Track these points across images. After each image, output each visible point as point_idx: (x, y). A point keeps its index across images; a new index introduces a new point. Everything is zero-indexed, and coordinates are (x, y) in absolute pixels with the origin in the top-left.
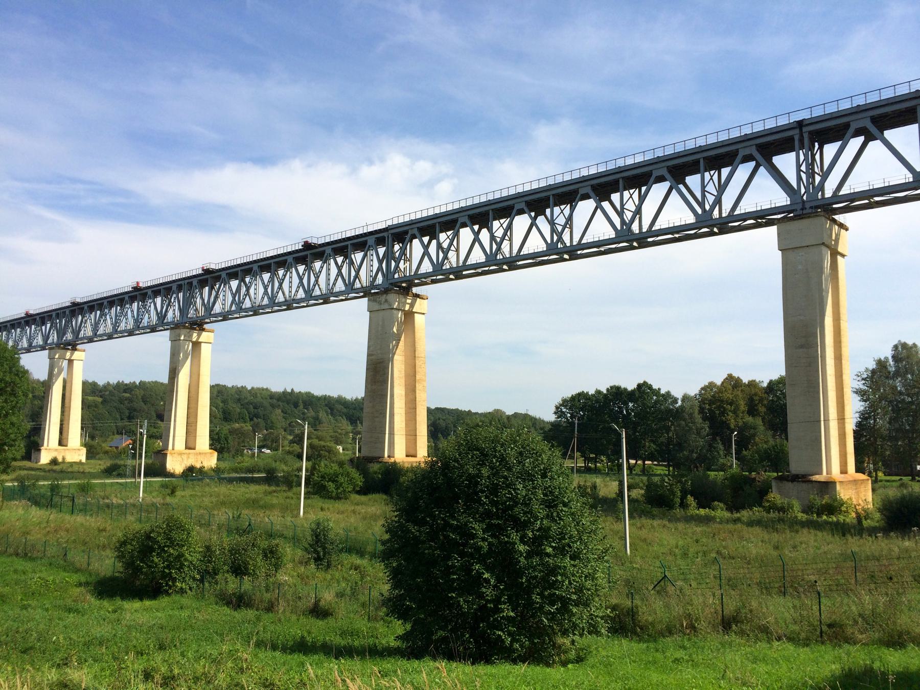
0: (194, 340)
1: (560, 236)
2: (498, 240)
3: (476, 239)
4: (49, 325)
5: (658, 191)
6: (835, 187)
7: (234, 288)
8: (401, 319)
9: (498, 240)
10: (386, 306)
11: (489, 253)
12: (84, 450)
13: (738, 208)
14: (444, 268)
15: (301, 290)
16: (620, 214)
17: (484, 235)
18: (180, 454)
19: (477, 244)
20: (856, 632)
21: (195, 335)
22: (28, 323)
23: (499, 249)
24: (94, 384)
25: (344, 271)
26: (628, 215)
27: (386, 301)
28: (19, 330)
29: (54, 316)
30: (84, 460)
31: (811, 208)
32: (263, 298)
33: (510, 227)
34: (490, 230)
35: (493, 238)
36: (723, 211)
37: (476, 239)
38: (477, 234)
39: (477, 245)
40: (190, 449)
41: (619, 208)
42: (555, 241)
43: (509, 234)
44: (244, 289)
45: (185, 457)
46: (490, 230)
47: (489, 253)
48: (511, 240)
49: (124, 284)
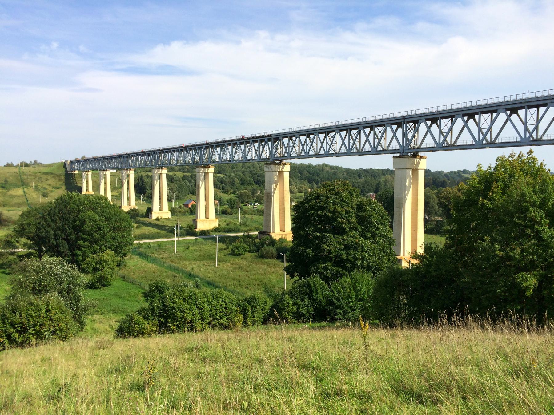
0: (206, 172)
1: (531, 134)
2: (445, 134)
3: (429, 131)
4: (151, 156)
5: (503, 117)
6: (433, 142)
7: (256, 147)
8: (202, 183)
9: (445, 134)
10: (270, 170)
11: (373, 146)
12: (170, 213)
13: (423, 145)
14: (378, 149)
15: (303, 151)
16: (525, 124)
17: (434, 128)
18: (203, 221)
19: (429, 134)
20: (9, 327)
21: (206, 169)
22: (182, 150)
23: (445, 140)
24: (429, 171)
25: (346, 141)
26: (531, 128)
27: (271, 168)
28: (170, 154)
29: (197, 148)
30: (170, 217)
31: (406, 152)
32: (255, 156)
33: (385, 131)
34: (439, 126)
35: (441, 132)
36: (545, 135)
37: (429, 131)
38: (429, 128)
39: (429, 134)
40: (207, 218)
41: (524, 120)
42: (527, 137)
43: (384, 136)
44: (261, 148)
45: (205, 222)
46: (439, 126)
47: (373, 146)
48: (385, 138)
49: (237, 135)
